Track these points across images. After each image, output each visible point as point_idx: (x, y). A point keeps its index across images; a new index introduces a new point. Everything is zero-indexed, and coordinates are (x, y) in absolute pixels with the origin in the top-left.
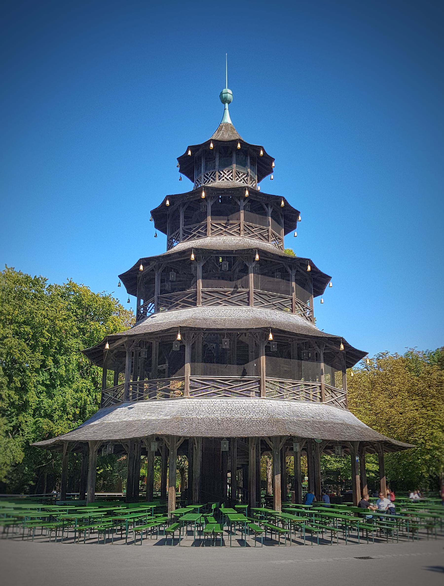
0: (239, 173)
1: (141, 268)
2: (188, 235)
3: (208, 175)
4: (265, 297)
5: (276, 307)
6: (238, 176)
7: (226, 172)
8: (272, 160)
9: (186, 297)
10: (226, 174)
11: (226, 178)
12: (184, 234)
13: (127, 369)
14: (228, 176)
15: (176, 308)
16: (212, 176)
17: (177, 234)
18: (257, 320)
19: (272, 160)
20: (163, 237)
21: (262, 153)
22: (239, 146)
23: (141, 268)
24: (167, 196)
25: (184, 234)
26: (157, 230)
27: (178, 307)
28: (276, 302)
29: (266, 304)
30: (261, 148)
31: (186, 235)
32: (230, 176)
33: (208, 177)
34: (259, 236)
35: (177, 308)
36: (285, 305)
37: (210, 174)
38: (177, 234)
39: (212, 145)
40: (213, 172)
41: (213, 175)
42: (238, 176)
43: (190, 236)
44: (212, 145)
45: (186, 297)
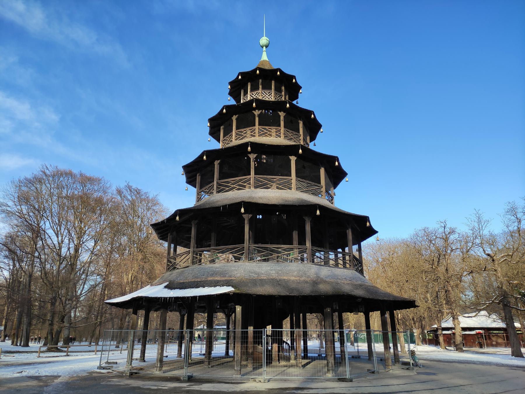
0: (276, 94)
1: (177, 218)
2: (240, 137)
3: (253, 95)
4: (304, 184)
5: (312, 193)
6: (276, 96)
7: (267, 93)
8: (300, 88)
9: (241, 182)
10: (267, 95)
11: (267, 97)
12: (237, 136)
13: (192, 238)
14: (268, 96)
15: (233, 190)
16: (256, 95)
17: (230, 136)
18: (302, 200)
19: (300, 88)
20: (193, 190)
21: (294, 81)
22: (278, 73)
23: (177, 218)
24: (225, 106)
25: (237, 136)
26: (188, 185)
27: (234, 190)
28: (311, 189)
29: (305, 190)
30: (294, 77)
31: (238, 136)
32: (270, 96)
33: (253, 96)
34: (295, 140)
35: (233, 191)
36: (318, 192)
37: (254, 94)
38: (230, 136)
39: (258, 72)
40: (258, 92)
41: (257, 95)
42: (276, 96)
43: (241, 137)
44: (258, 72)
45: (241, 182)
